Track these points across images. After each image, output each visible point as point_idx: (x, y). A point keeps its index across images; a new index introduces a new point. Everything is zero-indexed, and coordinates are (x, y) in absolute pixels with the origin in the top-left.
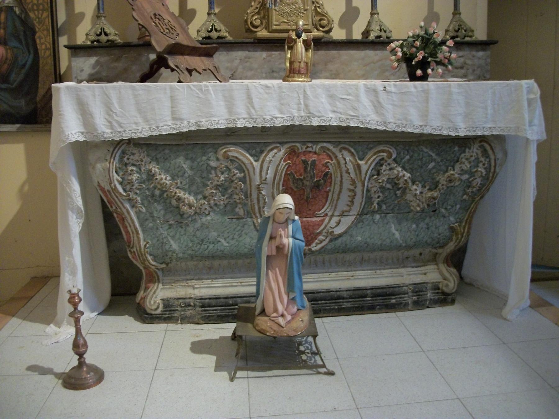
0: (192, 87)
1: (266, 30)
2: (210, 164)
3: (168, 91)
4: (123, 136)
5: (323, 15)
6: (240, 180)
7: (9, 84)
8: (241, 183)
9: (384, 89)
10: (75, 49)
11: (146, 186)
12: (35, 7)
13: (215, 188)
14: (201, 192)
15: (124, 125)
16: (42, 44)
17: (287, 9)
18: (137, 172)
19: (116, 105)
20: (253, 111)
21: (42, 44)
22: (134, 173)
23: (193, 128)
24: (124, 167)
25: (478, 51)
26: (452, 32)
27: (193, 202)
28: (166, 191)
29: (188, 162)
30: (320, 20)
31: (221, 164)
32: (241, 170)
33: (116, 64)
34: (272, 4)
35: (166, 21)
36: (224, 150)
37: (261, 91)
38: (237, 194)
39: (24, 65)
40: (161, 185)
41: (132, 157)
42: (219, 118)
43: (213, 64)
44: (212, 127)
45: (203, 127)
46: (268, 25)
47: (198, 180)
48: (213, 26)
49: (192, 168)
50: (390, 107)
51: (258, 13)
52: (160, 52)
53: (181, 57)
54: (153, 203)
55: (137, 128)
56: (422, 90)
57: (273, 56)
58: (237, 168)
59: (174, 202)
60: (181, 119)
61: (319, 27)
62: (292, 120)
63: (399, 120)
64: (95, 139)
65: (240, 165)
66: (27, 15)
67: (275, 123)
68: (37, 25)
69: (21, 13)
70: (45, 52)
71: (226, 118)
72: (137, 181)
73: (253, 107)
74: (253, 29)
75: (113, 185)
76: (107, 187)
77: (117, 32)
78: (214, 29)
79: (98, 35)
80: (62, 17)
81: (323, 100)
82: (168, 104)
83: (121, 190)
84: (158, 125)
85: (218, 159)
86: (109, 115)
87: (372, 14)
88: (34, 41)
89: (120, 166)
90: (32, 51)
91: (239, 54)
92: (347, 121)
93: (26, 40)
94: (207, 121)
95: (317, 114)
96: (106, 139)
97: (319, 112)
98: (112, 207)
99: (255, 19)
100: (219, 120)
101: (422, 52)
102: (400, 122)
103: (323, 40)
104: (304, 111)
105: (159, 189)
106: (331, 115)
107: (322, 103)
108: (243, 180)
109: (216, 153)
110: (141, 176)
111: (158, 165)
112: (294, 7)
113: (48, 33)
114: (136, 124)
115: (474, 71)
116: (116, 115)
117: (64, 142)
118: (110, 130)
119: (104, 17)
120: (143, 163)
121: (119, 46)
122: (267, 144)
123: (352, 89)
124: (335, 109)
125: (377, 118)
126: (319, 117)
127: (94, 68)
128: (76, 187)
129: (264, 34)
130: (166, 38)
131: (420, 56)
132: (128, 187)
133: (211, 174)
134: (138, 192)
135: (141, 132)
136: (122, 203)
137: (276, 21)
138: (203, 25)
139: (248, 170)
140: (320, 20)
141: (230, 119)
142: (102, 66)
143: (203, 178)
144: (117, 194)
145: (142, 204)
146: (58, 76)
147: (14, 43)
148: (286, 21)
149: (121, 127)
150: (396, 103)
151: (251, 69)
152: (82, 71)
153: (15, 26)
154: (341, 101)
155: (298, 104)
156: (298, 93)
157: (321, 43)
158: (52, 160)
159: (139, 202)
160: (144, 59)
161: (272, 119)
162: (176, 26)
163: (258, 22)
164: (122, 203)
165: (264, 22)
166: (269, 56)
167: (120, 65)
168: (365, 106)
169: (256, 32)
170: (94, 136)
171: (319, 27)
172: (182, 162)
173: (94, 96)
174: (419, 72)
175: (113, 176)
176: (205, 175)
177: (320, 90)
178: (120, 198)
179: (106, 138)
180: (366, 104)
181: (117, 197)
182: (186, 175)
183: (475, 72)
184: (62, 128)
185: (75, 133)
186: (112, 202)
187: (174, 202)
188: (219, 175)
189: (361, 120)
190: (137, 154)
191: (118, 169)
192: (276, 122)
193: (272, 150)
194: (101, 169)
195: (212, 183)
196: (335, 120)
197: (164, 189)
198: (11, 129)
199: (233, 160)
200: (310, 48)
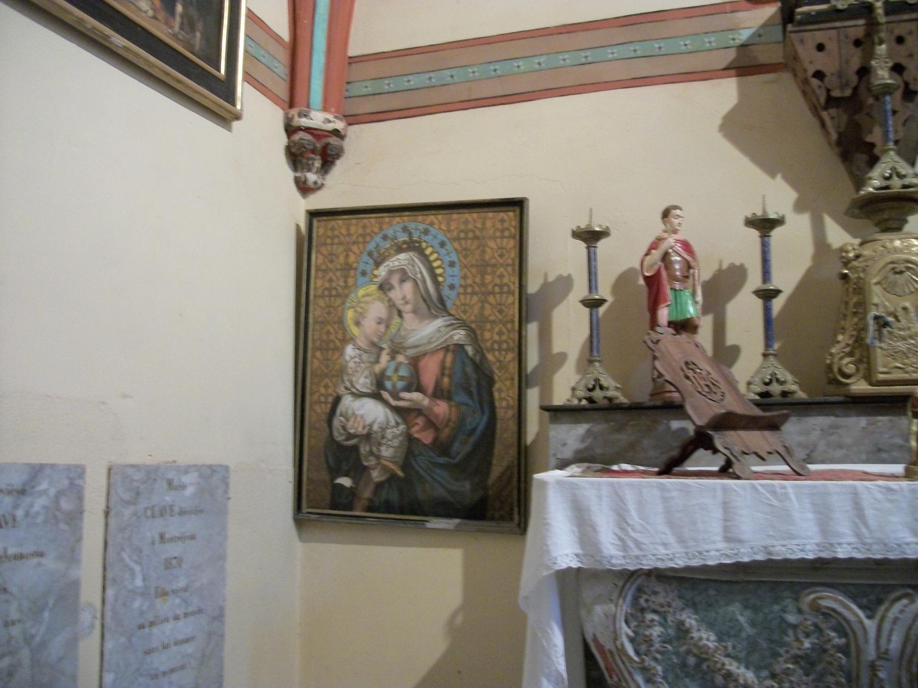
0: (760, 488)
2: (787, 619)
3: (719, 494)
4: (641, 564)
6: (840, 649)
7: (450, 457)
8: (840, 655)
10: (556, 413)
11: (674, 647)
12: (496, 346)
13: (794, 660)
14: (766, 667)
15: (644, 546)
16: (502, 399)
17: (901, 346)
18: (661, 625)
19: (634, 513)
20: (864, 530)
21: (502, 399)
22: (656, 625)
23: (760, 557)
24: (639, 614)
27: (753, 682)
28: (706, 660)
29: (748, 613)
31: (806, 619)
32: (842, 632)
35: (704, 373)
36: (812, 596)
37: (879, 496)
38: (832, 674)
39: (473, 430)
40: (700, 648)
41: (653, 598)
42: (805, 541)
43: (782, 442)
44: (793, 557)
45: (778, 555)
47: (764, 645)
48: (773, 375)
49: (753, 624)
51: (850, 354)
52: (701, 427)
53: (732, 433)
54: (682, 678)
55: (664, 552)
57: (880, 424)
58: (834, 629)
59: (719, 680)
60: (741, 541)
64: (598, 567)
65: (839, 623)
66: (483, 357)
67: (904, 553)
68: (496, 371)
69: (475, 355)
70: (506, 412)
71: (817, 541)
72: (659, 639)
73: (866, 525)
75: (618, 643)
76: (608, 645)
77: (618, 386)
79: (590, 390)
80: (532, 359)
82: (718, 513)
83: (631, 651)
84: (700, 549)
85: (800, 611)
86: (622, 529)
88: (491, 394)
89: (633, 612)
90: (487, 410)
91: (819, 422)
93: (479, 394)
94: (784, 546)
96: (614, 566)
98: (611, 677)
99: (847, 364)
100: (804, 545)
105: (695, 655)
108: (845, 650)
109: (797, 599)
110: (666, 630)
111: (696, 614)
112: (913, 342)
113: (512, 384)
114: (665, 545)
116: (633, 530)
117: (548, 568)
118: (621, 554)
120: (671, 610)
121: (623, 409)
122: (889, 588)
127: (582, 441)
128: (558, 639)
130: (707, 403)
132: (643, 648)
133: (787, 635)
134: (659, 656)
135: (671, 560)
136: (630, 673)
138: (757, 373)
139: (854, 632)
141: (823, 543)
142: (595, 438)
143: (771, 641)
144: (624, 658)
145: (664, 678)
147: (461, 397)
149: (641, 549)
151: (841, 447)
152: (564, 445)
153: (465, 374)
158: (523, 593)
159: (659, 675)
160: (661, 428)
161: (899, 545)
163: (850, 369)
164: (630, 673)
166: (873, 424)
167: (624, 438)
169: (847, 384)
170: (597, 561)
172: (737, 613)
173: (600, 497)
175: (621, 628)
176: (776, 637)
178: (628, 664)
179: (613, 565)
181: (623, 663)
182: (744, 635)
184: (546, 545)
185: (567, 555)
186: (614, 670)
187: (719, 680)
188: (801, 636)
190: (663, 594)
191: (629, 616)
192: (908, 551)
193: (898, 599)
194: (602, 615)
195: (787, 652)
197: (704, 656)
198: (447, 525)
199: (828, 614)
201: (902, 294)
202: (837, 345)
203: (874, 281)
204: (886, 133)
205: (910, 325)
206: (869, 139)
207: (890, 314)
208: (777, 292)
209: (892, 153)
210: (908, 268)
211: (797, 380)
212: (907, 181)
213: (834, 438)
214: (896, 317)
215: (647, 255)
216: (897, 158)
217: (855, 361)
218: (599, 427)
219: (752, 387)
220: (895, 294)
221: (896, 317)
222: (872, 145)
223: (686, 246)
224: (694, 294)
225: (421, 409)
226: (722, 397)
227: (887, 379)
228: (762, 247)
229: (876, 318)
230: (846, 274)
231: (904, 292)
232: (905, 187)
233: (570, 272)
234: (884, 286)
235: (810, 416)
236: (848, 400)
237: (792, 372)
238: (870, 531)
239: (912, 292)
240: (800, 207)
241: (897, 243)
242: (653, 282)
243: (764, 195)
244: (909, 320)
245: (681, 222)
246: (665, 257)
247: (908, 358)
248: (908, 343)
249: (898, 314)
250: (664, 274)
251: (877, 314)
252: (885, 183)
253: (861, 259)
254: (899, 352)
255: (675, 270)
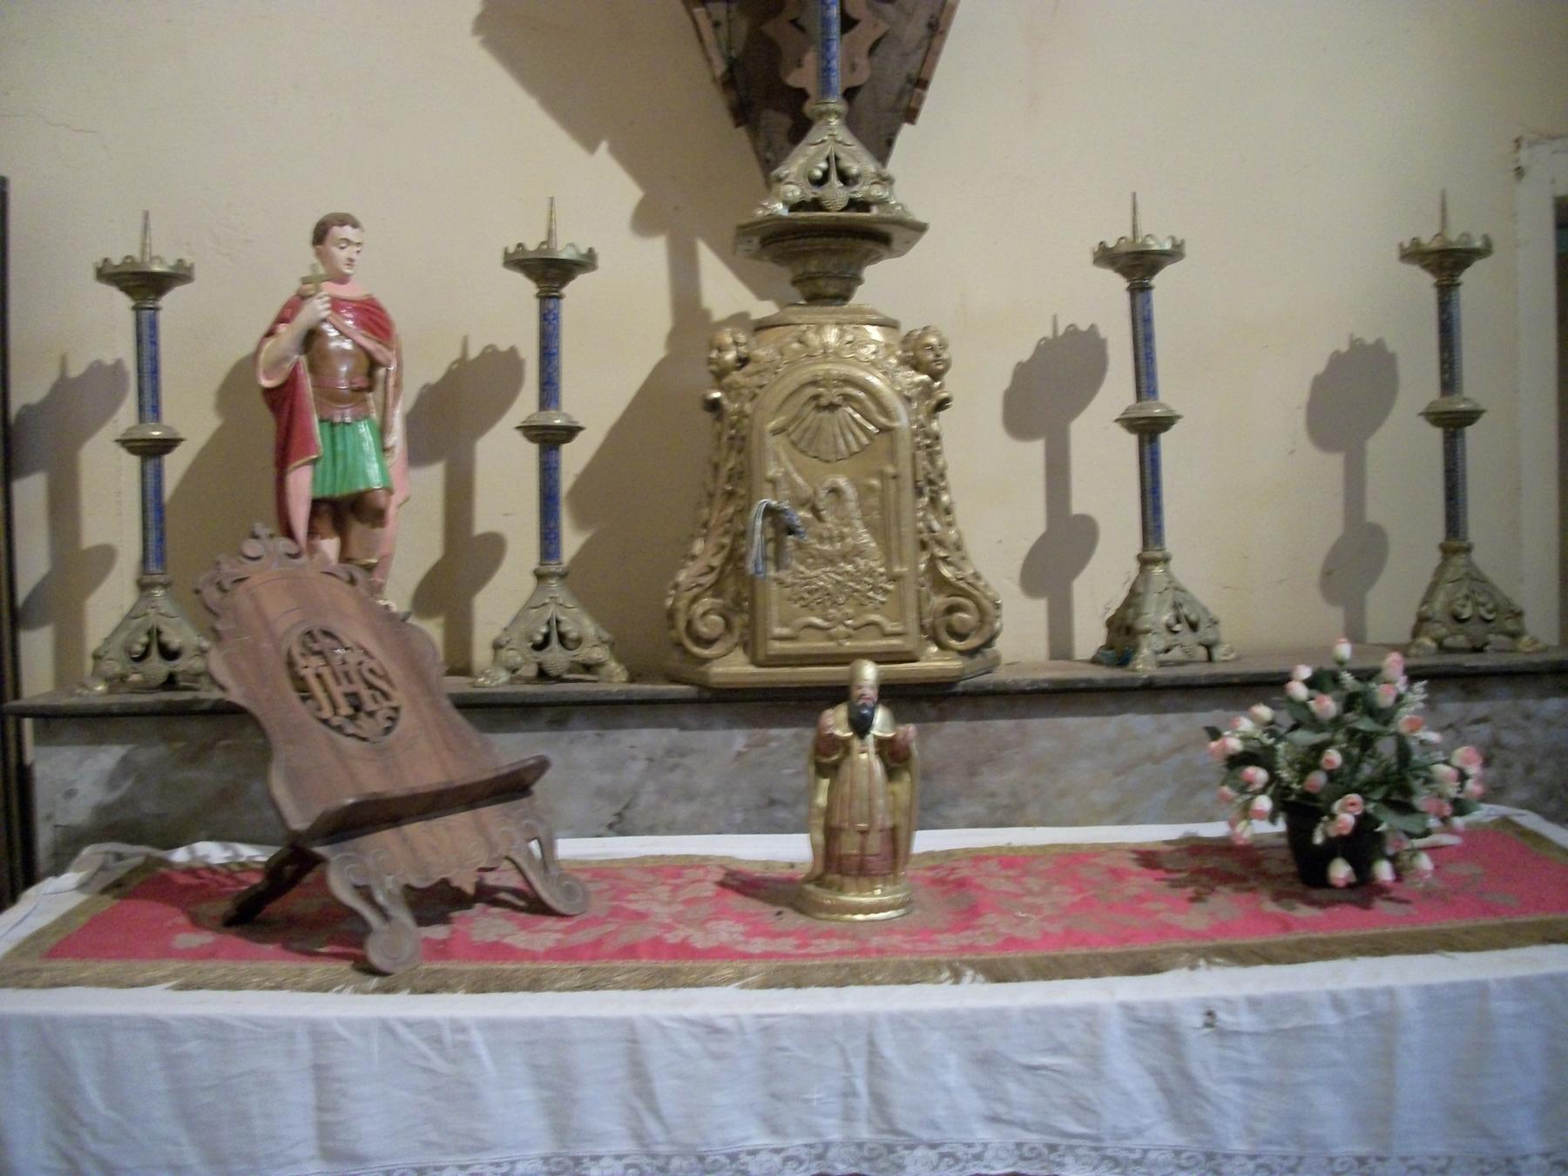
1: (745, 651)
5: (968, 596)
9: (1209, 1020)
17: (824, 577)
20: (652, 1125)
25: (1543, 696)
26: (1444, 625)
30: (951, 609)
33: (191, 774)
34: (765, 558)
42: (515, 1154)
46: (753, 633)
50: (1231, 1091)
52: (297, 835)
56: (1365, 1018)
57: (774, 745)
61: (944, 637)
62: (820, 1157)
63: (1270, 1142)
73: (656, 1113)
74: (697, 650)
78: (555, 636)
81: (952, 1078)
86: (68, 1133)
87: (1145, 562)
92: (1053, 1157)
95: (926, 1135)
97: (934, 1125)
99: (705, 614)
100: (513, 1163)
101: (1355, 797)
102: (1275, 1148)
103: (959, 688)
104: (870, 1121)
106: (983, 1134)
107: (947, 1089)
112: (849, 568)
115: (1529, 769)
119: (165, 586)
123: (1069, 1026)
124: (1001, 1109)
125: (1179, 1141)
126: (933, 1146)
129: (734, 669)
131: (1345, 817)
137: (779, 634)
138: (516, 620)
140: (951, 609)
146: (13, 774)
148: (818, 621)
150: (1256, 1074)
151: (690, 796)
152: (70, 794)
154: (1027, 1076)
155: (845, 1095)
156: (843, 1051)
157: (955, 695)
161: (733, 1157)
162: (395, 671)
163: (711, 625)
165: (739, 621)
166: (757, 745)
168: (1125, 1093)
169: (705, 661)
171: (944, 637)
174: (1340, 871)
177: (937, 1036)
180: (1130, 1086)
183: (1535, 774)
189: (1109, 1152)
196: (1003, 1154)
200: (907, 769)
201: (831, 457)
202: (691, 564)
203: (772, 424)
204: (825, 72)
205: (846, 530)
206: (794, 79)
207: (802, 504)
208: (570, 432)
209: (834, 122)
210: (848, 398)
211: (606, 636)
212: (859, 191)
213: (676, 777)
214: (815, 511)
215: (270, 333)
216: (843, 134)
217: (724, 607)
218: (150, 754)
219: (503, 653)
220: (815, 457)
221: (815, 511)
222: (802, 95)
223: (373, 317)
224: (382, 431)
225: (729, 82)
226: (388, 724)
227: (787, 652)
228: (541, 321)
229: (769, 511)
230: (716, 401)
231: (837, 452)
232: (853, 204)
233: (119, 356)
234: (793, 437)
235: (621, 727)
236: (707, 695)
237: (597, 618)
238: (667, 1129)
239: (852, 454)
240: (645, 221)
241: (831, 336)
242: (282, 399)
243: (552, 198)
244: (845, 520)
245: (354, 256)
246: (312, 339)
247: (835, 604)
248: (839, 571)
249: (821, 505)
250: (307, 383)
251: (774, 503)
252: (811, 193)
253: (749, 368)
254: (817, 590)
255: (335, 374)
